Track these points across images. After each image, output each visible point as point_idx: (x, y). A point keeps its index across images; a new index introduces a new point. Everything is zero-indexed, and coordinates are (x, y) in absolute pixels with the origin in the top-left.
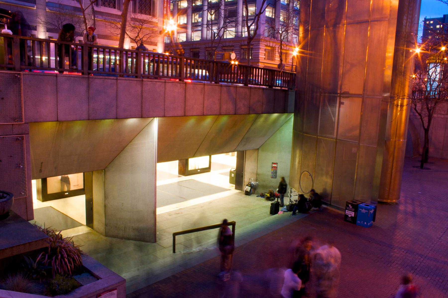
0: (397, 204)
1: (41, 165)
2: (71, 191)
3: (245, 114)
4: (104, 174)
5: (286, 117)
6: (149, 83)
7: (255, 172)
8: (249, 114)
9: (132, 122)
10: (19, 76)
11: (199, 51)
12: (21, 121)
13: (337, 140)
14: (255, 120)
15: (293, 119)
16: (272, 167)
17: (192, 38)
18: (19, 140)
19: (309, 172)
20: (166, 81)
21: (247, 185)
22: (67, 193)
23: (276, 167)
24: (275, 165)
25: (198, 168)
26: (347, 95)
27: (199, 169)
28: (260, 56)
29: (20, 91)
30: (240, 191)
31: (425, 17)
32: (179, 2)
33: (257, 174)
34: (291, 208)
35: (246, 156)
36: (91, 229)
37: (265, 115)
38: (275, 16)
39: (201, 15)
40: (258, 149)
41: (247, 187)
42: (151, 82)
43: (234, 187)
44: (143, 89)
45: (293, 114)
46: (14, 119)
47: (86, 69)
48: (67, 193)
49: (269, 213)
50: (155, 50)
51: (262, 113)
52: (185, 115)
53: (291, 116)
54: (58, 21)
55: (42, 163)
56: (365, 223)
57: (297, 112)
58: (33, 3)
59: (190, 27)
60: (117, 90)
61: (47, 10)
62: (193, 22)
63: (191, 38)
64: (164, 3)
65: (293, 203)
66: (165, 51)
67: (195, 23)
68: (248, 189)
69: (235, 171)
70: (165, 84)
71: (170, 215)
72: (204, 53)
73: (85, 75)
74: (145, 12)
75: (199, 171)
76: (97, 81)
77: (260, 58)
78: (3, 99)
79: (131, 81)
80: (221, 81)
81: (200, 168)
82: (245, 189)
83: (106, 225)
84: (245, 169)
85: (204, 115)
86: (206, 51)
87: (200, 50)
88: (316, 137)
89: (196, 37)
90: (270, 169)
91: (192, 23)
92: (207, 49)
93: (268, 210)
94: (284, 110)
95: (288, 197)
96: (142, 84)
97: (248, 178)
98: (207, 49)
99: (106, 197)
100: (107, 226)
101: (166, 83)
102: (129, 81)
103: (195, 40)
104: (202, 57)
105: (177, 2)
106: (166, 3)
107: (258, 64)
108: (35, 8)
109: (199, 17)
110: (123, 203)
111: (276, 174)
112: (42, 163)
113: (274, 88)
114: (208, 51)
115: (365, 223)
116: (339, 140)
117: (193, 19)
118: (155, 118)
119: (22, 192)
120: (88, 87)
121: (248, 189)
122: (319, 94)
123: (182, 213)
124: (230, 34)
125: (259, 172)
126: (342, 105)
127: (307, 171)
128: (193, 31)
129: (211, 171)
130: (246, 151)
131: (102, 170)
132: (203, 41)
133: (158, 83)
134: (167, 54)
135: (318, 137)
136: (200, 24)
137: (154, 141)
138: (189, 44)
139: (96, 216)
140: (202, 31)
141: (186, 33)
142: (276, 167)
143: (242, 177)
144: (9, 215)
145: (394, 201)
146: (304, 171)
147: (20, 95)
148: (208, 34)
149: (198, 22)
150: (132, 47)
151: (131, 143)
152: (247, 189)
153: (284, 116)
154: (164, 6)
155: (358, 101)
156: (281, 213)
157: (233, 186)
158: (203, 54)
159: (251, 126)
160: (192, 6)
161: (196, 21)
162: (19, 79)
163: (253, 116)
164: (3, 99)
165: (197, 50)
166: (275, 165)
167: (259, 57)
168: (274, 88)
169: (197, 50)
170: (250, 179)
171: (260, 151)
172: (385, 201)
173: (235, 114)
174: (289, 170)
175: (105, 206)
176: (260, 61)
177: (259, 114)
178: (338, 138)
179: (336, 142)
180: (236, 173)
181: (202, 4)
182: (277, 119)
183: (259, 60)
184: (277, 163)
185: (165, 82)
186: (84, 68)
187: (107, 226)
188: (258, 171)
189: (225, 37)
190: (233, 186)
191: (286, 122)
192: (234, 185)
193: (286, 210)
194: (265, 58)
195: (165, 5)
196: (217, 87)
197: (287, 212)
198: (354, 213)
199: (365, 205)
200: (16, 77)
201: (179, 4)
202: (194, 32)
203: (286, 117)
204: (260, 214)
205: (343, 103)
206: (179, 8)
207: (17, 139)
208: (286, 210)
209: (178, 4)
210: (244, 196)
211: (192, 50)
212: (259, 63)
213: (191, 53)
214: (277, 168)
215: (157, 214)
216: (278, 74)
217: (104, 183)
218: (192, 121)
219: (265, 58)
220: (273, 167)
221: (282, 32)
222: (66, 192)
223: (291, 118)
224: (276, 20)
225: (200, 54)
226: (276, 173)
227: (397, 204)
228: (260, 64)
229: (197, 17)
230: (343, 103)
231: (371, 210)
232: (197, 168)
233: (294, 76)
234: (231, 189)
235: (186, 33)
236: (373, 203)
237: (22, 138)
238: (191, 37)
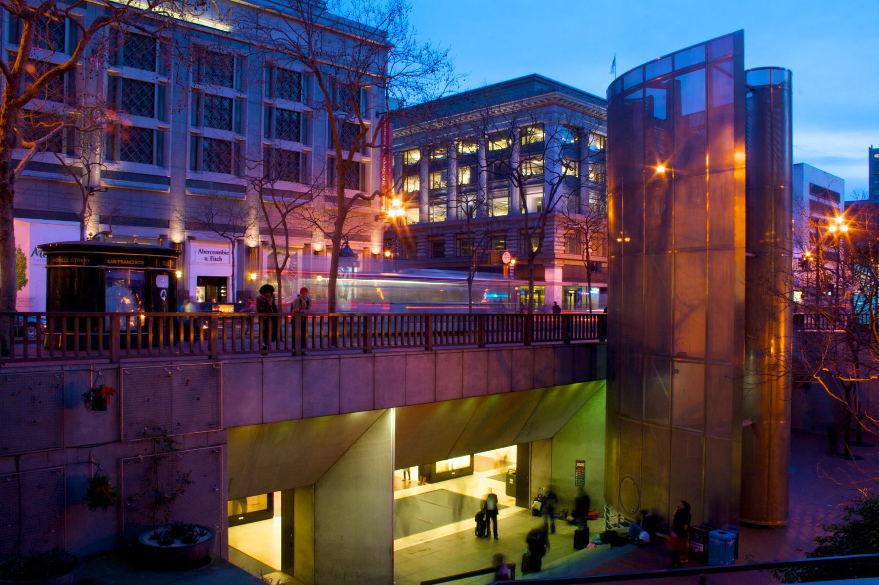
0: (784, 527)
1: (230, 482)
2: (249, 513)
3: (526, 390)
4: (314, 492)
5: (596, 385)
6: (383, 359)
7: (549, 476)
8: (534, 388)
9: (357, 416)
10: (217, 368)
11: (444, 240)
12: (218, 427)
13: (673, 429)
14: (544, 396)
15: (605, 389)
16: (576, 468)
17: (431, 216)
18: (215, 453)
19: (632, 479)
20: (408, 353)
21: (536, 499)
22: (242, 518)
23: (583, 468)
24: (581, 465)
25: (452, 468)
26: (685, 357)
27: (453, 471)
28: (556, 248)
29: (218, 386)
30: (524, 509)
31: (870, 147)
32: (406, 153)
33: (551, 480)
34: (609, 537)
35: (533, 450)
36: (291, 577)
37: (559, 387)
38: (579, 175)
39: (445, 176)
40: (552, 438)
41: (535, 502)
42: (386, 358)
43: (514, 502)
44: (376, 368)
45: (605, 381)
46: (210, 425)
47: (298, 347)
48: (242, 518)
49: (572, 546)
50: (367, 249)
51: (555, 385)
52: (436, 401)
53: (600, 386)
54: (207, 214)
55: (232, 479)
56: (721, 562)
57: (611, 377)
58: (167, 184)
59: (425, 198)
60: (340, 374)
61: (188, 193)
62: (432, 188)
63: (429, 217)
64: (381, 168)
65: (611, 529)
66: (385, 248)
67: (434, 190)
68: (537, 505)
69: (514, 474)
70: (406, 359)
71: (412, 554)
72: (454, 244)
73: (298, 356)
74: (349, 185)
75: (453, 473)
76: (315, 363)
77: (555, 251)
78: (198, 399)
79: (358, 359)
80: (488, 343)
81: (455, 468)
82: (533, 506)
83: (316, 570)
84: (532, 472)
85: (463, 398)
86: (457, 239)
87: (445, 239)
88: (640, 422)
89: (438, 215)
90: (574, 470)
91: (430, 190)
92: (458, 237)
93: (571, 542)
94: (590, 376)
95: (604, 517)
96: (374, 361)
97: (537, 486)
98: (458, 237)
99: (316, 526)
100: (317, 572)
101: (407, 356)
102: (356, 359)
103: (435, 220)
104: (449, 252)
105: (403, 154)
106: (384, 167)
107: (552, 262)
108: (169, 192)
109: (443, 179)
110: (342, 536)
111: (584, 479)
112: (232, 479)
113: (572, 342)
114: (460, 239)
115: (721, 562)
116: (675, 428)
117: (432, 183)
118: (392, 409)
119: (215, 525)
120: (302, 373)
121: (537, 505)
122: (640, 356)
123: (430, 549)
124: (500, 208)
125: (555, 476)
126: (676, 375)
127: (630, 478)
128: (431, 204)
129: (474, 473)
130: (533, 443)
131: (311, 486)
132: (450, 224)
133: (396, 358)
134: (388, 254)
135: (644, 423)
136: (444, 191)
137: (390, 441)
138: (424, 228)
139: (298, 556)
140: (448, 202)
141: (418, 209)
142: (583, 468)
143: (527, 484)
144: (211, 559)
145: (779, 522)
146: (627, 477)
147: (218, 394)
148: (459, 210)
149: (440, 189)
150: (327, 246)
151: (356, 444)
152: (535, 505)
153: (592, 384)
154: (381, 172)
155: (699, 369)
156: (590, 548)
157: (512, 500)
158: (452, 245)
159: (538, 405)
160: (430, 159)
161: (437, 187)
162: (218, 371)
163: (539, 391)
164: (198, 399)
165: (441, 238)
166: (581, 465)
167: (553, 250)
168: (572, 342)
169: (441, 238)
170: (540, 488)
171: (555, 441)
172: (763, 523)
173: (511, 391)
174: (603, 472)
175: (315, 541)
176: (556, 256)
177: (548, 386)
178: (673, 426)
179: (671, 432)
180: (517, 477)
181: (448, 157)
182: (578, 393)
183: (554, 254)
184: (584, 461)
185: (406, 355)
186: (296, 346)
187: (317, 572)
188: (553, 475)
189: (490, 214)
190: (512, 500)
191: (596, 393)
192: (514, 499)
193: (599, 542)
194: (564, 251)
195: (384, 170)
196: (482, 353)
197: (600, 544)
198: (702, 545)
199: (720, 533)
200: (214, 369)
201: (406, 156)
202: (434, 207)
203: (596, 385)
204: (557, 549)
205: (677, 372)
206: (406, 163)
207: (213, 452)
208: (599, 542)
209: (403, 156)
210: (531, 517)
211: (430, 239)
212: (554, 261)
213: (430, 243)
214: (584, 469)
215: (395, 550)
216: (578, 320)
217: (314, 505)
218: (444, 407)
219: (564, 251)
220: (577, 468)
221: (588, 228)
222: (241, 516)
223: (600, 388)
224: (583, 179)
225: (445, 246)
226: (583, 477)
227: (784, 527)
228: (556, 263)
229: (438, 178)
230: (677, 372)
231: (730, 541)
232: (450, 469)
233: (604, 319)
234: (508, 505)
235: (418, 209)
236: (732, 529)
237: (219, 450)
238: (429, 214)
